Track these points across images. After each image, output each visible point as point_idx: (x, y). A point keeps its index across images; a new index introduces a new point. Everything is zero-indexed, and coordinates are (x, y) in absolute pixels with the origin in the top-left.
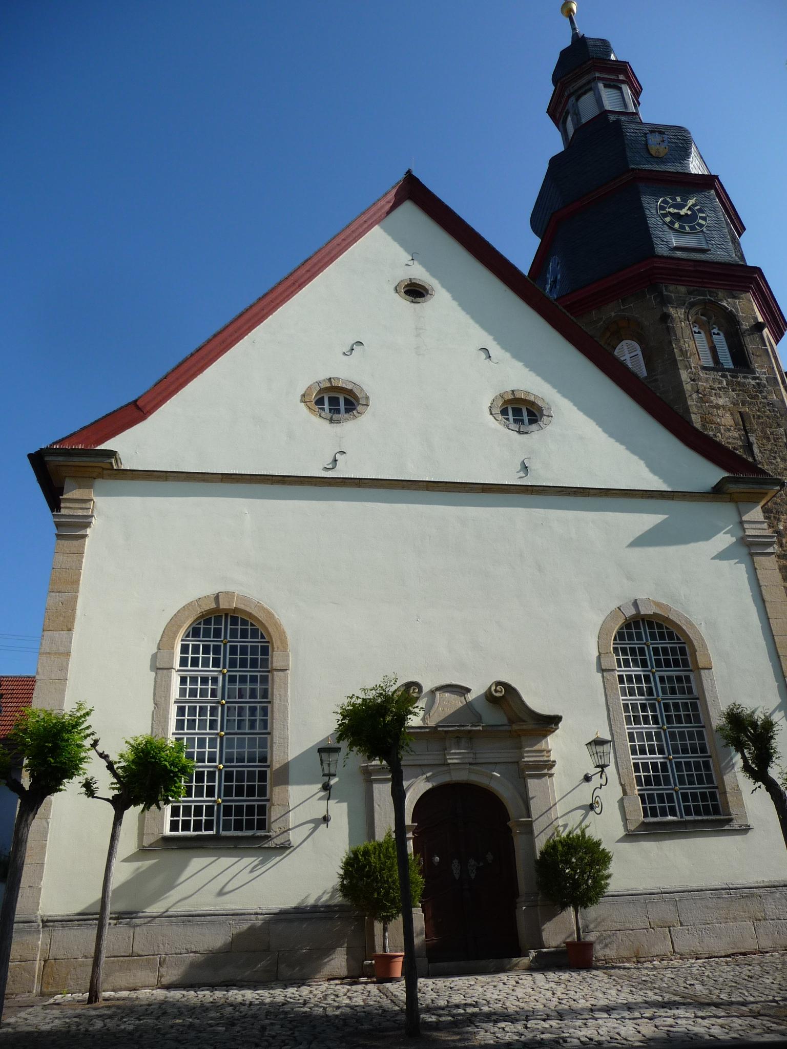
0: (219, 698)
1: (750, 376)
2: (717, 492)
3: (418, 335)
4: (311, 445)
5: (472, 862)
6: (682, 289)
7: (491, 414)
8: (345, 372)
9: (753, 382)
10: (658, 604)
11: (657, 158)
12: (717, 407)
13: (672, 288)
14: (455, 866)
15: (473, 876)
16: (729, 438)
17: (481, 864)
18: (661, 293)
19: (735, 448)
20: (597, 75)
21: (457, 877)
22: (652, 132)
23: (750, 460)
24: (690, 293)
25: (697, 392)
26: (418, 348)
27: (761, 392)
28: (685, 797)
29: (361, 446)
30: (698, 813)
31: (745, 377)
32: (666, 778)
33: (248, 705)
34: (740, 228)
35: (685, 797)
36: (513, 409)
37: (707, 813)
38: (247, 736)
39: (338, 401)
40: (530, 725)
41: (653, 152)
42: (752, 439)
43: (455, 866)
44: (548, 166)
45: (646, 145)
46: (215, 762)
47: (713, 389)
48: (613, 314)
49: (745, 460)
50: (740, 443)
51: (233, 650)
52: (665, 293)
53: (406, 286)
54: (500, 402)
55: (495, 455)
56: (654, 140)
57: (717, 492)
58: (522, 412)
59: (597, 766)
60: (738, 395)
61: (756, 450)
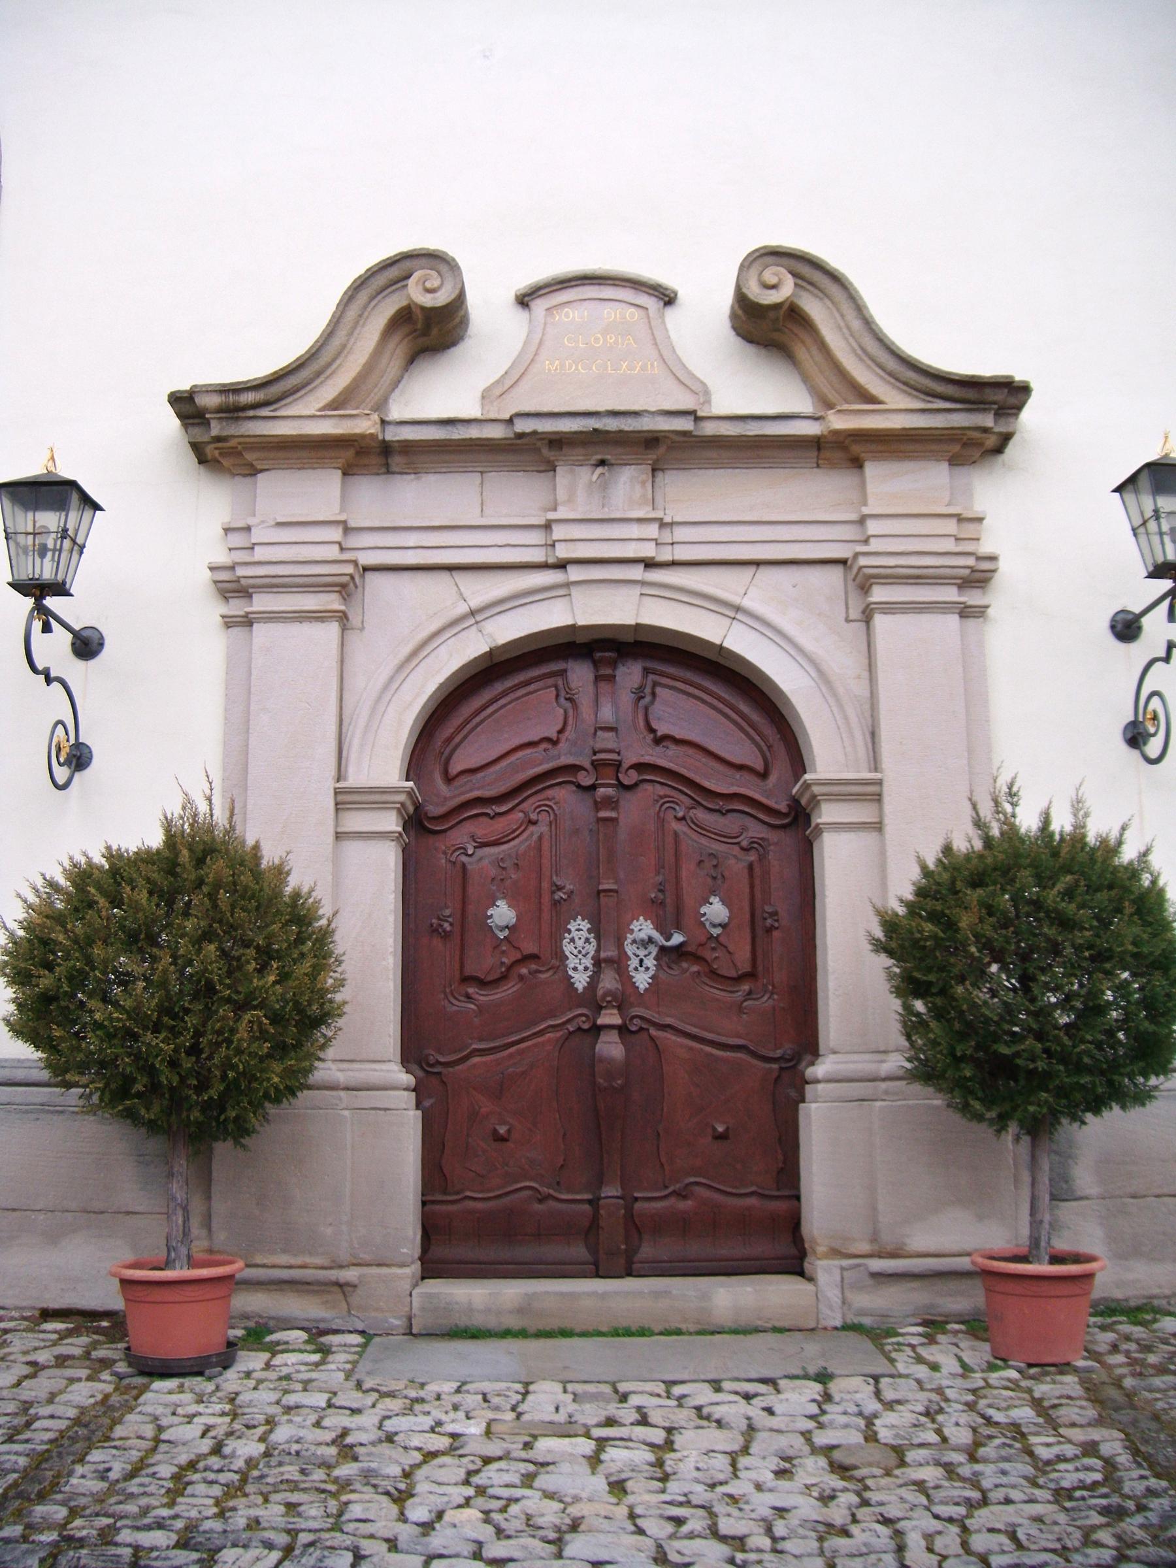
5: (643, 928)
14: (578, 946)
17: (677, 939)
21: (580, 980)
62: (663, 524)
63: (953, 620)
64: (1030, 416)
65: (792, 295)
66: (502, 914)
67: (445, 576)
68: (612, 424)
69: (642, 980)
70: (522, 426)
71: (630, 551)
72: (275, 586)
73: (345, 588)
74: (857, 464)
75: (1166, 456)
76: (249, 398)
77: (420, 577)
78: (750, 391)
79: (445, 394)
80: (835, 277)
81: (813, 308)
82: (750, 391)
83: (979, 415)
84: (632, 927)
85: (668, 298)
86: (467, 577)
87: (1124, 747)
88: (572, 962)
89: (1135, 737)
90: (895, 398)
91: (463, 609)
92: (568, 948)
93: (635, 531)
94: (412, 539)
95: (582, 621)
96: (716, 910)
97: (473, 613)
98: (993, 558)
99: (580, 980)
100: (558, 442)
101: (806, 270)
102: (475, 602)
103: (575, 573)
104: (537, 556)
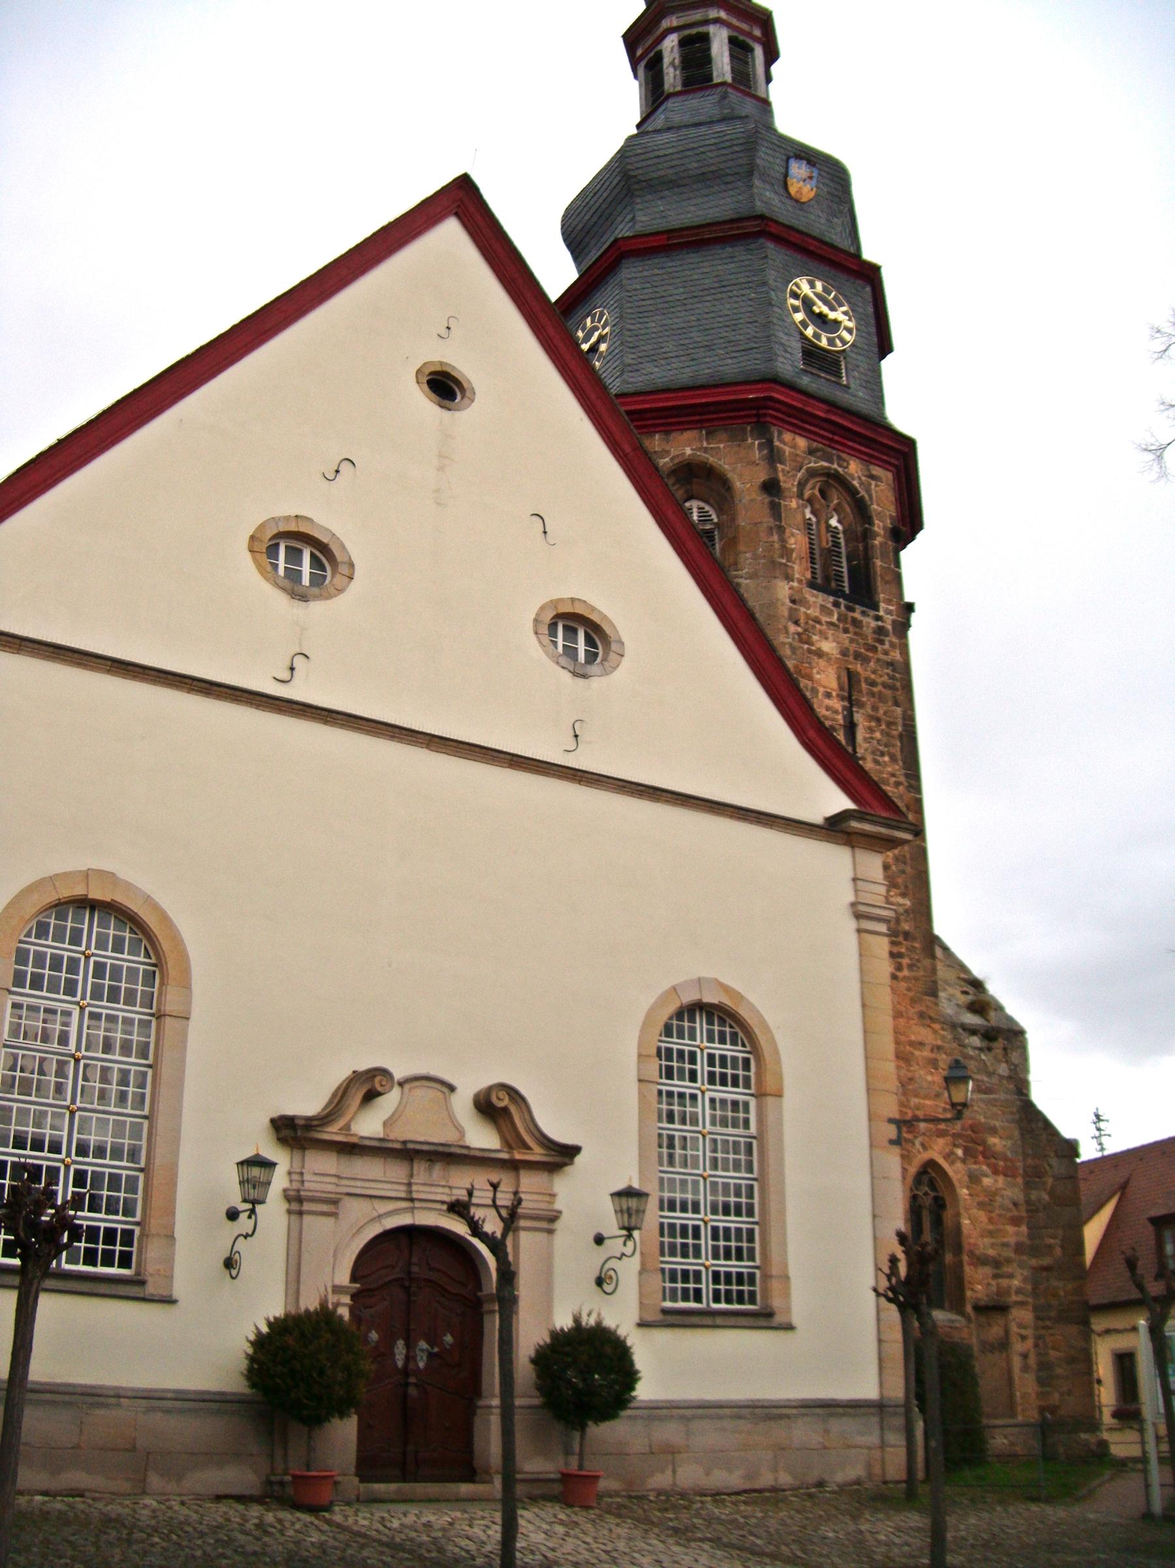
0: (72, 1046)
1: (872, 613)
2: (834, 829)
3: (441, 468)
4: (252, 629)
5: (423, 1345)
6: (802, 442)
7: (536, 633)
8: (328, 517)
9: (873, 624)
10: (727, 989)
11: (797, 201)
12: (820, 654)
13: (788, 436)
14: (400, 1349)
15: (421, 1365)
16: (828, 708)
17: (436, 1350)
18: (770, 443)
19: (833, 728)
20: (723, 14)
21: (400, 1364)
22: (798, 157)
23: (850, 749)
24: (811, 452)
25: (796, 623)
26: (438, 491)
27: (882, 642)
28: (716, 1276)
29: (333, 648)
30: (729, 1301)
31: (863, 613)
32: (697, 1249)
33: (116, 1066)
34: (885, 347)
35: (716, 1276)
36: (564, 627)
37: (740, 1300)
38: (112, 1117)
39: (302, 556)
40: (538, 1154)
41: (793, 190)
42: (858, 717)
43: (400, 1349)
44: (909, 546)
45: (786, 175)
46: (59, 1152)
47: (819, 622)
48: (688, 451)
49: (846, 750)
50: (840, 717)
51: (99, 969)
52: (777, 443)
53: (431, 373)
54: (551, 614)
55: (534, 702)
56: (798, 170)
57: (834, 829)
58: (580, 634)
59: (623, 1228)
60: (852, 641)
61: (860, 735)
62: (450, 1188)
63: (545, 1235)
64: (578, 1159)
65: (551, 1182)
66: (374, 1336)
67: (368, 1200)
68: (441, 1149)
69: (421, 1365)
70: (410, 1146)
71: (438, 1198)
72: (313, 1200)
73: (335, 1202)
74: (412, 1160)
75: (258, 1155)
76: (315, 1123)
77: (360, 1200)
78: (482, 1137)
79: (369, 1124)
80: (523, 1099)
81: (513, 1109)
82: (482, 1137)
83: (563, 1155)
84: (859, 755)
85: (452, 1088)
86: (379, 1204)
87: (594, 1284)
88: (397, 1357)
89: (600, 1282)
90: (537, 1149)
91: (375, 1214)
92: (396, 1351)
93: (441, 1190)
94: (359, 1184)
95: (417, 1223)
96: (449, 1339)
97: (380, 1216)
98: (560, 1212)
99: (400, 1364)
100: (436, 1153)
101: (512, 1093)
102: (381, 1211)
103: (417, 1204)
104: (403, 1195)
